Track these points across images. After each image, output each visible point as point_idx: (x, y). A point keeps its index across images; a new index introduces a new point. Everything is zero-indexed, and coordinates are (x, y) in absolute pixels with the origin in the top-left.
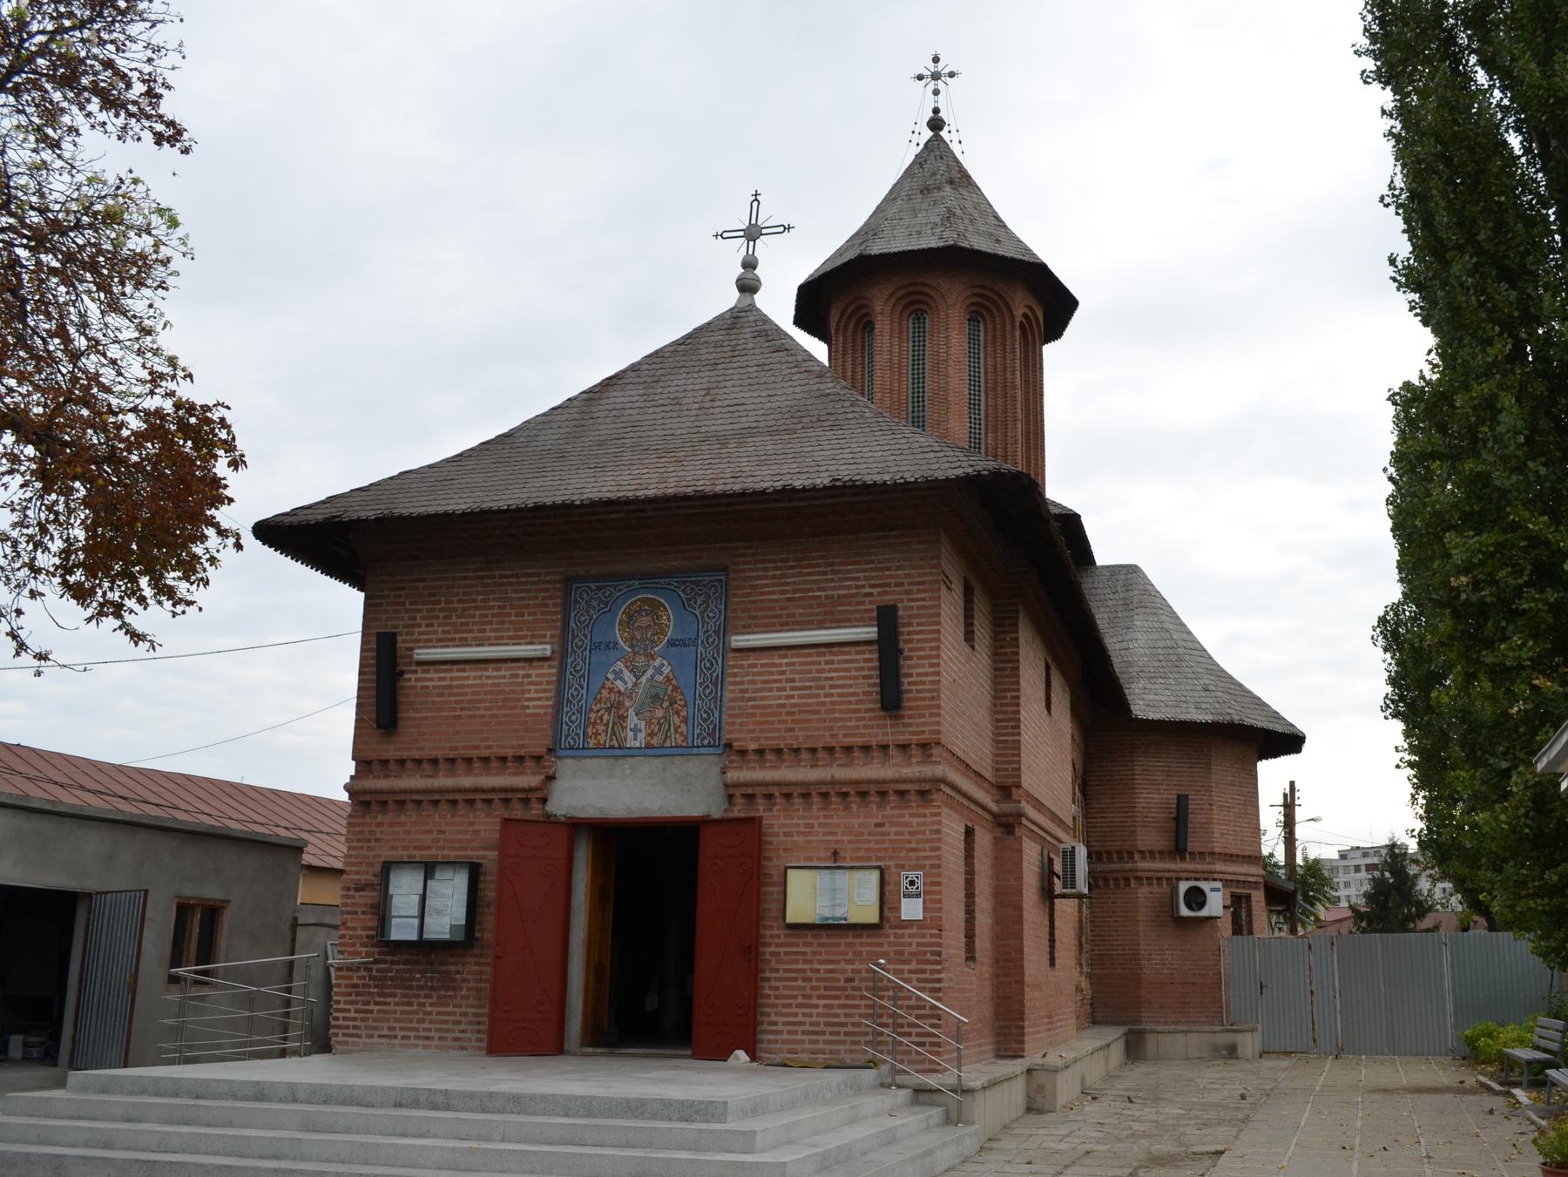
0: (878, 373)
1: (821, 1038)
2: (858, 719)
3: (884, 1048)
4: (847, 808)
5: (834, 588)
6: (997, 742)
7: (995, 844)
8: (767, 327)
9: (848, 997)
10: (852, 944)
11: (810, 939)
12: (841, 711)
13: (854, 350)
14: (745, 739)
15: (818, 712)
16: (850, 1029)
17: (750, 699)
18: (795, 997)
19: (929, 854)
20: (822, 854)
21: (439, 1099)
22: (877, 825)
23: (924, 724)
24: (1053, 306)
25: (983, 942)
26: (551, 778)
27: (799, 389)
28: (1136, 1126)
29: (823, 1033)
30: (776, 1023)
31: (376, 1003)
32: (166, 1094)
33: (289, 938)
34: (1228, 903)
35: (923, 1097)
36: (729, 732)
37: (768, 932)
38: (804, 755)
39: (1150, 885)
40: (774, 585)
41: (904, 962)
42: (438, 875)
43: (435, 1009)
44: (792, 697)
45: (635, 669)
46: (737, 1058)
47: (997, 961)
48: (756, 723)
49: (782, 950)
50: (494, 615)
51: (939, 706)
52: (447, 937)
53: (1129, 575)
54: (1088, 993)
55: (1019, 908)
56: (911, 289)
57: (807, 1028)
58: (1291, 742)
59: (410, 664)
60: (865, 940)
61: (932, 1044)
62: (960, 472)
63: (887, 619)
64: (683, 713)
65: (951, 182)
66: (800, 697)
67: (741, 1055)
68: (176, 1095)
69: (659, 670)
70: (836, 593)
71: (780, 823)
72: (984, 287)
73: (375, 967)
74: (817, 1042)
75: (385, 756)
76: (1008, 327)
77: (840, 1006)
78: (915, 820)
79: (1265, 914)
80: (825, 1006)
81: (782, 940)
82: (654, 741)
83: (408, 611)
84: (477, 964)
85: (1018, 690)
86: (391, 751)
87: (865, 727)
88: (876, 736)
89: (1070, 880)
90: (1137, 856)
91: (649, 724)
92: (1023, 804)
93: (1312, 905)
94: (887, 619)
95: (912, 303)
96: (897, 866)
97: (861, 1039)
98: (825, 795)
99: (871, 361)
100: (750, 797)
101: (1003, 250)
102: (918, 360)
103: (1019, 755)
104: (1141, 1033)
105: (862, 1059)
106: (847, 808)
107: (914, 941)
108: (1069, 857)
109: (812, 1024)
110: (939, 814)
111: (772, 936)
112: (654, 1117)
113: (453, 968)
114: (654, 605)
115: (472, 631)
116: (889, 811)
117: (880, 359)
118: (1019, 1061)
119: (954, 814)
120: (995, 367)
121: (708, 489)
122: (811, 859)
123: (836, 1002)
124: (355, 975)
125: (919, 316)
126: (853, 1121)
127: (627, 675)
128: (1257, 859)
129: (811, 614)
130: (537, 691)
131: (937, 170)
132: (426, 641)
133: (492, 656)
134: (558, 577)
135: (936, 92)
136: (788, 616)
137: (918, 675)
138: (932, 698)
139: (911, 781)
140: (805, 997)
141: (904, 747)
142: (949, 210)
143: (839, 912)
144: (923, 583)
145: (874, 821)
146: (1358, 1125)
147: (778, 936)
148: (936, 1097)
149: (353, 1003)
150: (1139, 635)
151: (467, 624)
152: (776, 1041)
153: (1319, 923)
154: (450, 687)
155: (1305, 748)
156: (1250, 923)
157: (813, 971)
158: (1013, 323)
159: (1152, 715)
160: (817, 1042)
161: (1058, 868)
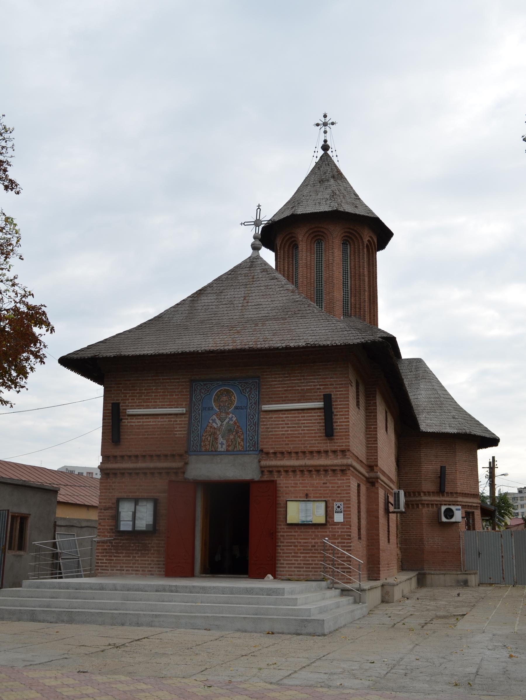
0: (301, 269)
1: (302, 570)
2: (315, 440)
3: (328, 574)
4: (311, 477)
5: (305, 386)
6: (367, 447)
7: (367, 490)
8: (266, 267)
9: (313, 553)
10: (314, 532)
11: (297, 530)
12: (309, 437)
13: (288, 257)
14: (268, 448)
15: (299, 437)
16: (314, 566)
17: (270, 432)
18: (291, 553)
19: (345, 495)
20: (301, 495)
21: (173, 589)
22: (324, 483)
23: (343, 442)
24: (383, 235)
25: (363, 532)
26: (186, 464)
27: (284, 298)
28: (428, 607)
29: (303, 568)
30: (283, 564)
31: (115, 556)
32: (64, 588)
33: (53, 531)
34: (464, 515)
35: (345, 593)
36: (261, 445)
37: (279, 527)
38: (293, 455)
39: (428, 507)
40: (279, 384)
41: (335, 539)
42: (140, 504)
43: (140, 559)
44: (288, 431)
45: (221, 420)
46: (269, 578)
47: (368, 540)
48: (273, 441)
49: (285, 534)
50: (160, 396)
51: (349, 435)
52: (145, 529)
53: (418, 363)
54: (400, 556)
55: (378, 517)
56: (315, 230)
57: (296, 565)
58: (493, 441)
59: (125, 416)
60: (319, 530)
61: (347, 572)
62: (359, 341)
63: (328, 399)
64: (242, 437)
65: (333, 177)
66: (291, 431)
67: (270, 576)
68: (68, 589)
69: (231, 419)
70: (305, 388)
71: (284, 483)
72: (349, 228)
73: (114, 542)
74: (300, 571)
75: (116, 454)
76: (361, 247)
77: (309, 557)
78: (339, 482)
79: (481, 521)
80: (303, 557)
81: (285, 530)
82: (230, 449)
83: (123, 393)
84: (158, 540)
85: (376, 425)
86: (117, 452)
87: (318, 443)
88: (323, 447)
89: (397, 504)
90: (422, 494)
91: (227, 441)
92: (379, 473)
93: (503, 517)
94: (328, 399)
95: (315, 236)
96: (332, 500)
97: (319, 570)
98: (302, 471)
99: (297, 262)
100: (271, 472)
101: (359, 211)
102: (319, 262)
103: (377, 453)
104: (425, 574)
105: (319, 578)
106: (311, 477)
107: (340, 530)
108: (397, 496)
109: (298, 564)
110: (349, 479)
111: (281, 528)
112: (257, 594)
113: (147, 542)
114: (228, 392)
115: (151, 402)
116: (329, 478)
117: (302, 262)
118: (378, 581)
119: (354, 479)
120: (355, 265)
121: (255, 346)
122: (297, 497)
123: (308, 555)
124: (105, 545)
125: (319, 242)
126: (323, 599)
127: (218, 421)
128: (477, 495)
129: (295, 397)
130: (179, 428)
131: (326, 172)
132: (131, 406)
133: (158, 411)
134: (187, 380)
135: (325, 132)
136: (286, 397)
137: (340, 422)
138: (346, 432)
139: (338, 466)
140: (295, 553)
141: (334, 452)
142: (333, 192)
143: (309, 519)
144: (342, 384)
145: (322, 482)
146: (521, 607)
147: (284, 529)
148: (351, 593)
149: (105, 556)
150: (422, 392)
151: (149, 399)
152: (283, 571)
153: (507, 526)
154: (142, 425)
155: (500, 444)
156: (474, 525)
157: (298, 542)
158: (363, 245)
159: (429, 430)
160: (300, 571)
161: (391, 500)
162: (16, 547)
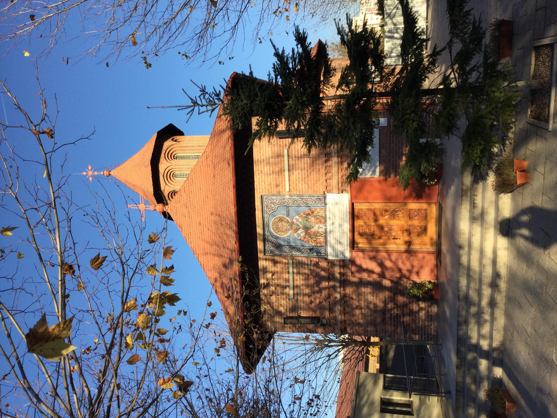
162: (383, 407)
